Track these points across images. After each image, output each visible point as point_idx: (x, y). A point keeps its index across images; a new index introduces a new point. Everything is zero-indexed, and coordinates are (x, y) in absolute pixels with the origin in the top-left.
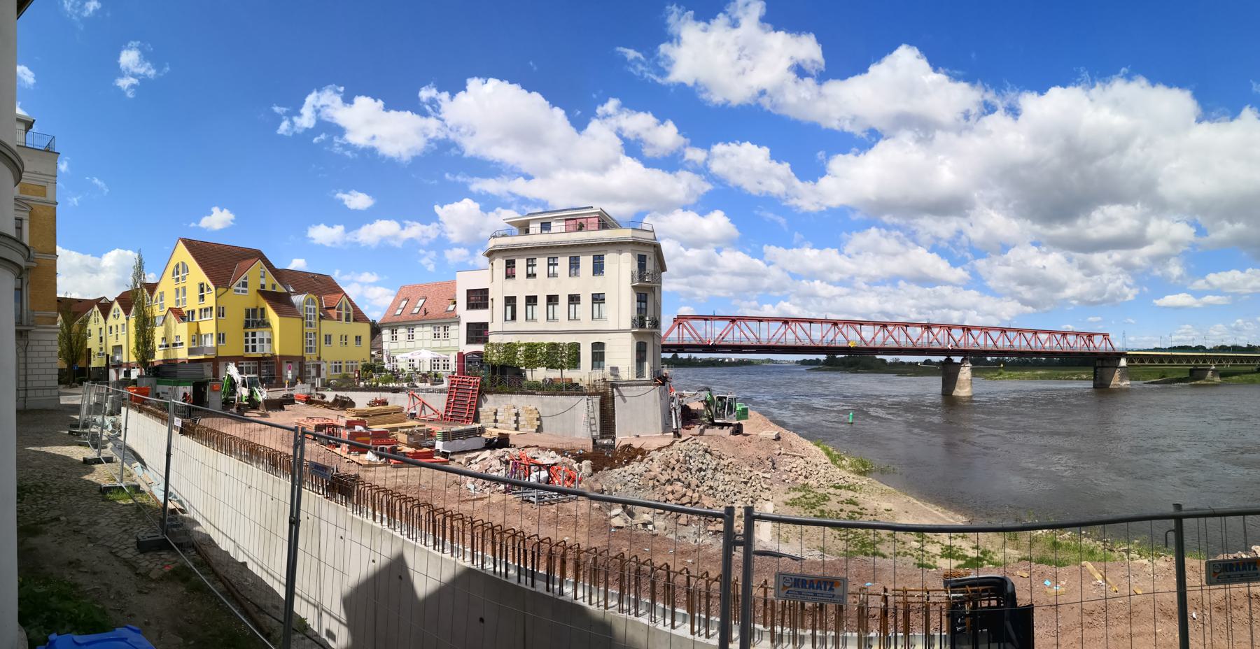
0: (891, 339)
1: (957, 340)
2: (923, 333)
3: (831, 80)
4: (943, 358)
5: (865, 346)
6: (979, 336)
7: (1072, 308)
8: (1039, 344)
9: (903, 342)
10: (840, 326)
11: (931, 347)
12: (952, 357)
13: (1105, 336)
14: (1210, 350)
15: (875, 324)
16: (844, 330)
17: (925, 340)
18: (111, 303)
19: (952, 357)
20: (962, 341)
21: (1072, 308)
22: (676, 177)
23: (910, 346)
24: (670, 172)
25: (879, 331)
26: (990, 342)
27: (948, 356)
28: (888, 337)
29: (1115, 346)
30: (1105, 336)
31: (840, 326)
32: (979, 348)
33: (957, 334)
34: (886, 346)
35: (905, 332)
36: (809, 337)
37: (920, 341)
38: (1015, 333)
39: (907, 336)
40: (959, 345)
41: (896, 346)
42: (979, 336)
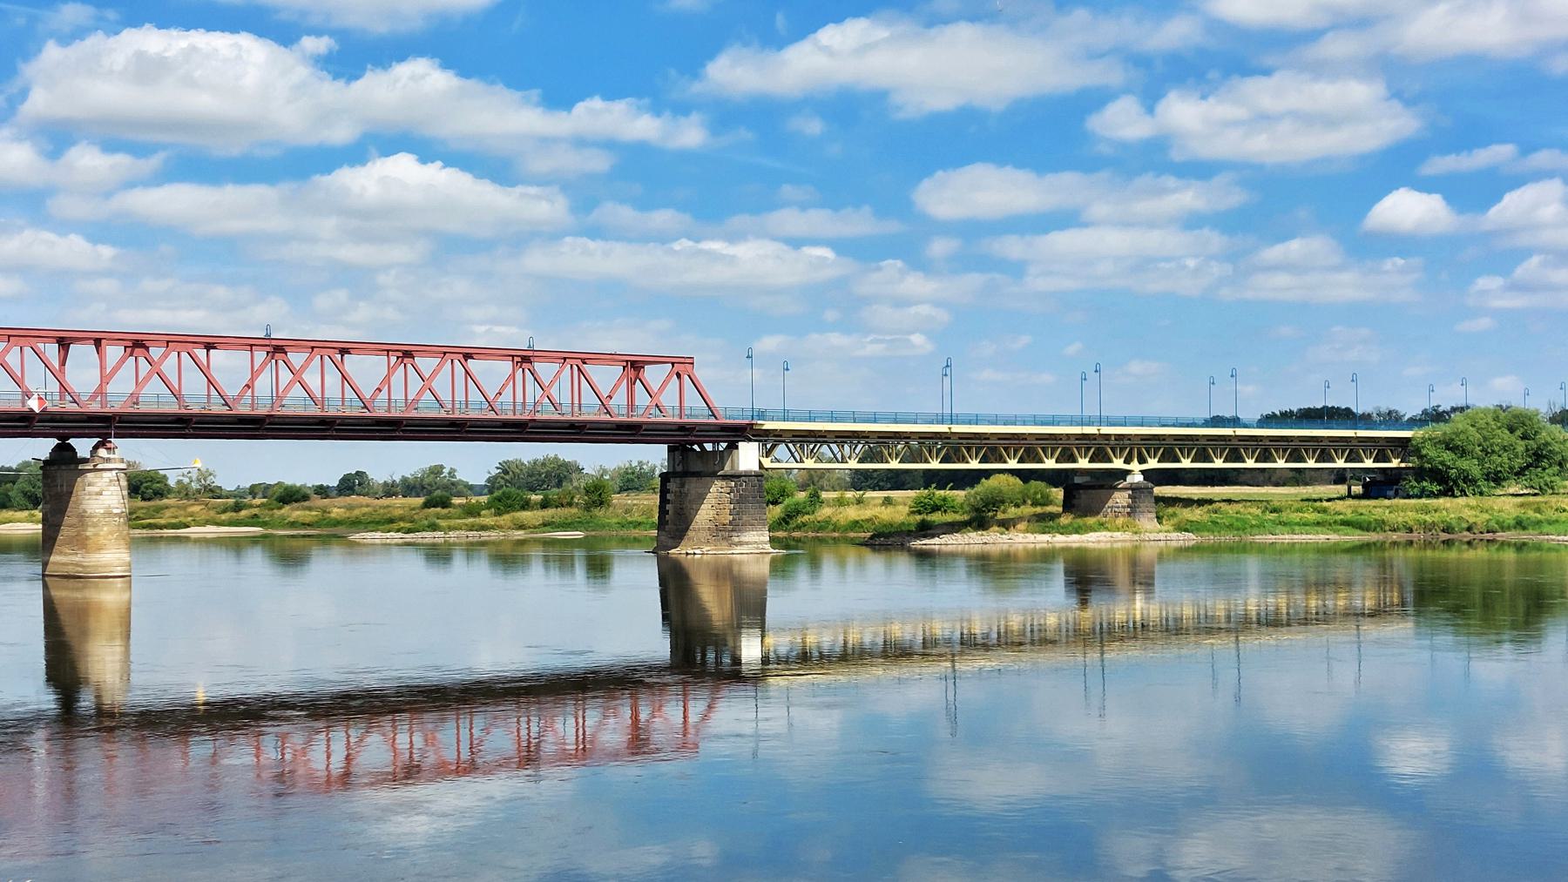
0: (297, 390)
1: (491, 396)
2: (391, 370)
3: (147, 25)
4: (42, 448)
5: (224, 410)
6: (435, 373)
7: (1484, 323)
8: (475, 396)
9: (196, 397)
10: (296, 358)
11: (414, 414)
12: (72, 441)
13: (681, 367)
14: (1413, 423)
15: (251, 345)
16: (169, 366)
17: (398, 395)
18: (781, 568)
19: (72, 441)
20: (507, 396)
21: (1484, 323)
22: (291, 50)
23: (217, 408)
24: (286, 46)
25: (122, 361)
26: (589, 398)
27: (63, 438)
28: (148, 378)
29: (717, 403)
30: (681, 367)
31: (156, 352)
32: (556, 417)
33: (494, 373)
34: (143, 408)
35: (204, 370)
36: (177, 396)
37: (384, 395)
38: (556, 367)
39: (467, 372)
40: (497, 407)
41: (172, 407)
42: (435, 373)
